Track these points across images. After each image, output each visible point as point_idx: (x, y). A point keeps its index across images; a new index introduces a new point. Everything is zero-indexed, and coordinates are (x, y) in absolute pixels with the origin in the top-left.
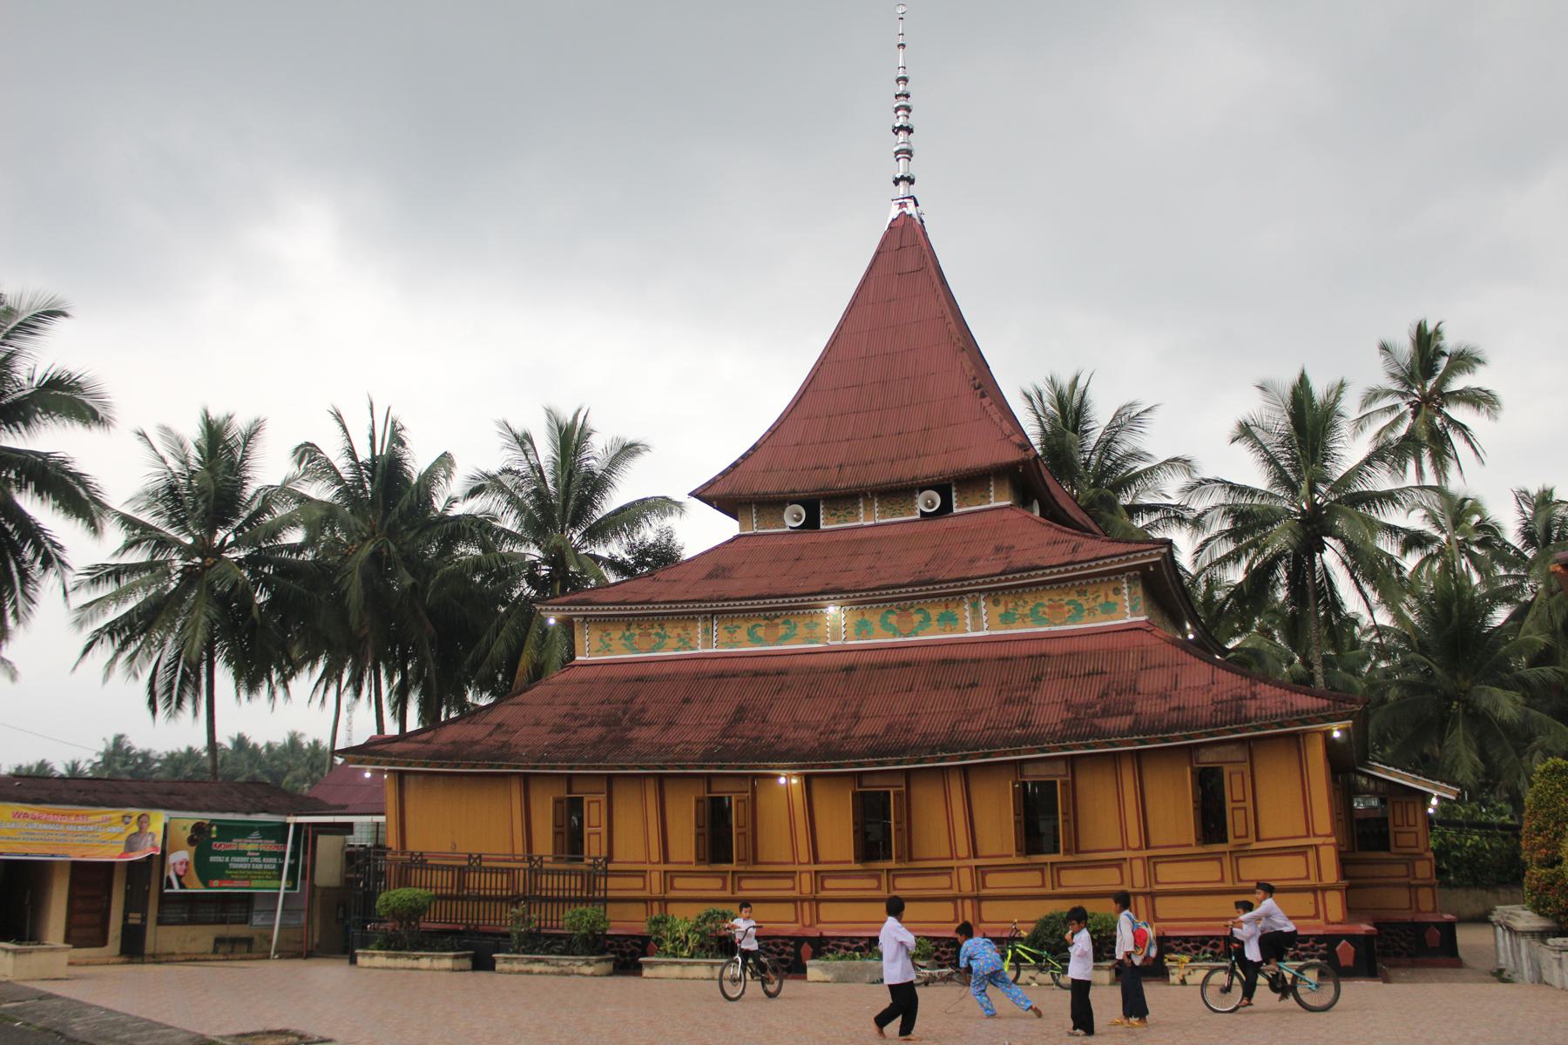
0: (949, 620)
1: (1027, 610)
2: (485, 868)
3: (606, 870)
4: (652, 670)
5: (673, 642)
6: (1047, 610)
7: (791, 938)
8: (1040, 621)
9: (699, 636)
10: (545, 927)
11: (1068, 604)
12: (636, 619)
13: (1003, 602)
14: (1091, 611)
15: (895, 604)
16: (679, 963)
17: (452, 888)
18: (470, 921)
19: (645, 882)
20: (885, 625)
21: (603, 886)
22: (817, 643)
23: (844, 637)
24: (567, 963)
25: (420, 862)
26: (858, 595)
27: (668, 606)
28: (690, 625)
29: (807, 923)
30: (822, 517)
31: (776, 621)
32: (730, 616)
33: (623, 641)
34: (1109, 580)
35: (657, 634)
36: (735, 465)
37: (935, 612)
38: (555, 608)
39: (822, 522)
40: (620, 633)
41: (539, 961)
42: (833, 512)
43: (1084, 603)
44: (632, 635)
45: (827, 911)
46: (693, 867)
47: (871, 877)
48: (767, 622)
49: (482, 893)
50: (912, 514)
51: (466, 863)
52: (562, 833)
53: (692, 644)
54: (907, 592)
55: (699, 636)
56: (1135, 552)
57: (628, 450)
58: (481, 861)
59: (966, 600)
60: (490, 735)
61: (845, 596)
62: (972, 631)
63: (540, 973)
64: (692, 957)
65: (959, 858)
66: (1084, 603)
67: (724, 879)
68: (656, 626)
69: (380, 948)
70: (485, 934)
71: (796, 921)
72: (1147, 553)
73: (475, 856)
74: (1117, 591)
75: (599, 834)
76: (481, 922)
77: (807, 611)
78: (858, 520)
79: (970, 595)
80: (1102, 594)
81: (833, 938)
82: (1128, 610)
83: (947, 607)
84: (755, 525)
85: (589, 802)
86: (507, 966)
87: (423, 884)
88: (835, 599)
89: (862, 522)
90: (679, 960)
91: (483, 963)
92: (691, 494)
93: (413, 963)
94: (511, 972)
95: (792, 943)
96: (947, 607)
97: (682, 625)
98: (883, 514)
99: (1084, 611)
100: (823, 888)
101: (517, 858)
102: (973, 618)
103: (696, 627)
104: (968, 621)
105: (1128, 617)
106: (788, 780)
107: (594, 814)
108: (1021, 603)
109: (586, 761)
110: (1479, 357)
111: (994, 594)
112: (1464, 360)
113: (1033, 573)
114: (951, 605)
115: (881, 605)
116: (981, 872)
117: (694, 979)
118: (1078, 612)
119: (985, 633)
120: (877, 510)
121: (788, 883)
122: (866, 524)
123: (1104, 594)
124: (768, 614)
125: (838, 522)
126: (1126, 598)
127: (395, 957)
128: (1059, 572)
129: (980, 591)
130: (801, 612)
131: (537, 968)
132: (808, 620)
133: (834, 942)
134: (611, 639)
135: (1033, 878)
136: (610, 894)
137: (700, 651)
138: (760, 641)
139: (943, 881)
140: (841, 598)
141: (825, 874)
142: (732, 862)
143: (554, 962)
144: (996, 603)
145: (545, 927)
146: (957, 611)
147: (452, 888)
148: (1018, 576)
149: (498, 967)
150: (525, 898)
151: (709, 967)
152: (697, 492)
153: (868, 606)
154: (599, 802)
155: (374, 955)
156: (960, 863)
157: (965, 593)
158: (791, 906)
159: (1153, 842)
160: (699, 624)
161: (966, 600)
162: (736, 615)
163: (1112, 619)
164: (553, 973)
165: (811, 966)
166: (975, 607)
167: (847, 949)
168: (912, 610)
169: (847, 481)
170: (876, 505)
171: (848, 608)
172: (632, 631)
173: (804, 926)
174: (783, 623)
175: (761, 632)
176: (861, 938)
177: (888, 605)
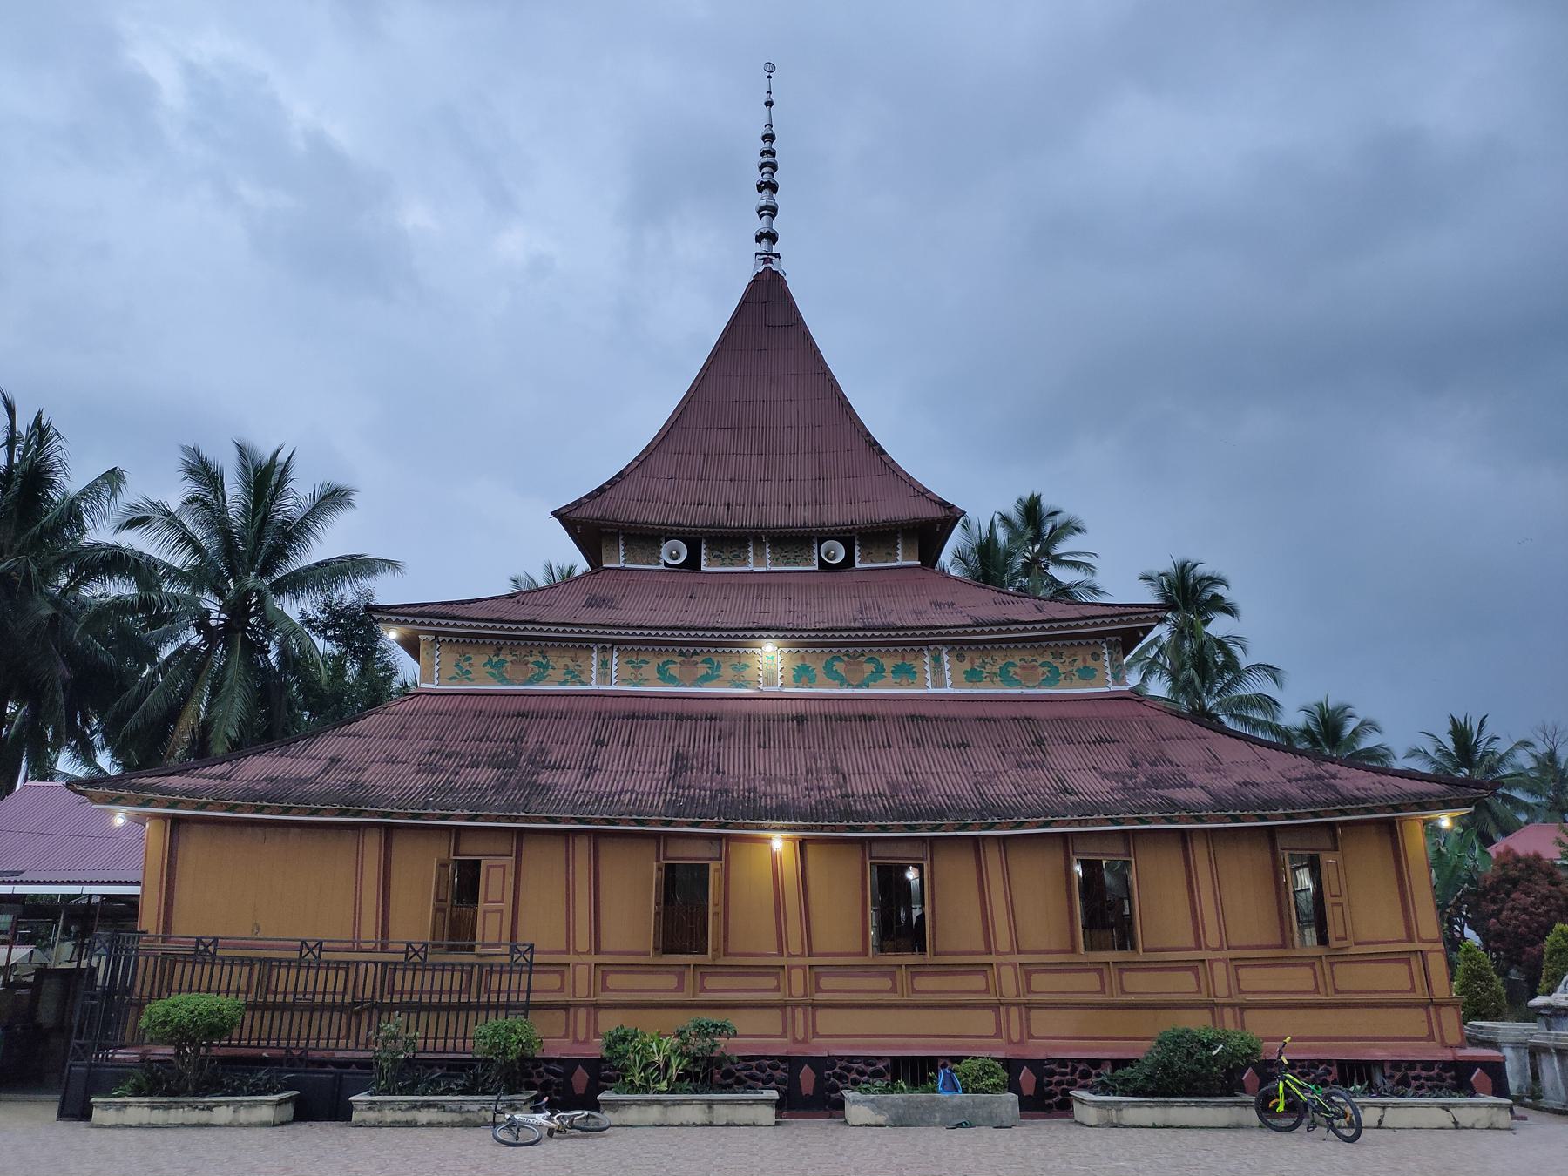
0: (905, 673)
1: (996, 669)
2: (223, 958)
3: (531, 964)
4: (533, 704)
5: (559, 674)
6: (1018, 670)
7: (783, 1059)
8: (1011, 682)
9: (594, 669)
10: (317, 1048)
11: (1042, 665)
12: (509, 643)
13: (968, 658)
14: (1068, 675)
15: (843, 650)
16: (659, 1102)
17: (344, 992)
18: (293, 1043)
19: (563, 981)
20: (830, 672)
21: (524, 987)
22: (746, 687)
23: (780, 682)
24: (476, 1107)
25: (203, 953)
26: (805, 635)
27: (561, 629)
28: (582, 655)
29: (800, 1036)
30: (703, 557)
31: (695, 658)
32: (636, 648)
33: (488, 668)
34: (1032, 646)
35: (537, 663)
36: (601, 490)
37: (889, 663)
38: (402, 619)
39: (703, 563)
40: (485, 659)
41: (429, 1105)
42: (717, 553)
43: (1060, 666)
44: (503, 662)
45: (828, 1021)
46: (651, 959)
47: (884, 975)
48: (683, 658)
49: (319, 998)
50: (808, 565)
51: (296, 955)
52: (444, 910)
53: (582, 678)
54: (865, 636)
55: (594, 669)
56: (1112, 616)
57: (333, 498)
58: (321, 950)
59: (926, 652)
60: (325, 771)
61: (789, 635)
62: (933, 687)
63: (430, 1125)
64: (673, 1092)
65: (998, 953)
66: (1060, 666)
67: (681, 976)
68: (535, 652)
69: (137, 1092)
70: (322, 1063)
71: (784, 1034)
72: (1142, 617)
73: (312, 944)
74: (1096, 656)
75: (501, 911)
76: (313, 1043)
77: (734, 650)
78: (745, 565)
79: (931, 647)
80: (1080, 658)
81: (841, 1058)
82: (1109, 678)
83: (903, 658)
84: (622, 559)
85: (489, 867)
86: (372, 1116)
87: (224, 987)
88: (775, 637)
89: (750, 567)
90: (650, 1096)
91: (339, 1112)
92: (555, 514)
93: (204, 1116)
94: (380, 1125)
95: (782, 1066)
96: (903, 658)
97: (572, 654)
98: (775, 561)
99: (1060, 675)
100: (605, 989)
101: (365, 946)
102: (934, 673)
103: (590, 658)
104: (928, 676)
105: (1110, 685)
106: (779, 843)
107: (494, 883)
108: (989, 660)
109: (498, 808)
110: (1079, 526)
111: (959, 648)
112: (1071, 528)
113: (1012, 628)
114: (907, 656)
115: (826, 650)
116: (1028, 969)
117: (681, 1125)
118: (1053, 677)
119: (948, 691)
120: (768, 556)
121: (770, 982)
122: (756, 569)
123: (1082, 658)
124: (684, 649)
125: (723, 565)
126: (1107, 664)
127: (167, 1107)
128: (1043, 629)
129: (944, 643)
130: (727, 650)
131: (424, 1116)
132: (735, 661)
133: (843, 1063)
134: (471, 665)
135: (1089, 981)
136: (534, 998)
137: (594, 686)
138: (672, 680)
139: (977, 982)
140: (784, 637)
141: (821, 970)
142: (706, 953)
143: (454, 1106)
144: (961, 658)
145: (317, 1048)
146: (915, 664)
147: (344, 992)
148: (995, 629)
149: (355, 1117)
150: (375, 1006)
151: (705, 1107)
152: (563, 512)
153: (810, 650)
154: (504, 867)
155: (125, 1105)
156: (1001, 959)
157: (927, 643)
158: (777, 1013)
159: (604, 946)
160: (594, 655)
161: (926, 652)
162: (643, 648)
163: (1092, 686)
164: (453, 1125)
165: (855, 1102)
166: (937, 660)
167: (862, 1073)
168: (862, 659)
169: (740, 519)
170: (768, 550)
171: (786, 650)
172: (501, 657)
173: (795, 1041)
174: (703, 662)
175: (674, 670)
176: (879, 1058)
177: (835, 650)
